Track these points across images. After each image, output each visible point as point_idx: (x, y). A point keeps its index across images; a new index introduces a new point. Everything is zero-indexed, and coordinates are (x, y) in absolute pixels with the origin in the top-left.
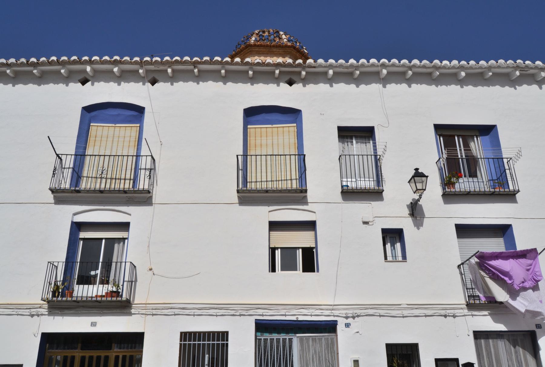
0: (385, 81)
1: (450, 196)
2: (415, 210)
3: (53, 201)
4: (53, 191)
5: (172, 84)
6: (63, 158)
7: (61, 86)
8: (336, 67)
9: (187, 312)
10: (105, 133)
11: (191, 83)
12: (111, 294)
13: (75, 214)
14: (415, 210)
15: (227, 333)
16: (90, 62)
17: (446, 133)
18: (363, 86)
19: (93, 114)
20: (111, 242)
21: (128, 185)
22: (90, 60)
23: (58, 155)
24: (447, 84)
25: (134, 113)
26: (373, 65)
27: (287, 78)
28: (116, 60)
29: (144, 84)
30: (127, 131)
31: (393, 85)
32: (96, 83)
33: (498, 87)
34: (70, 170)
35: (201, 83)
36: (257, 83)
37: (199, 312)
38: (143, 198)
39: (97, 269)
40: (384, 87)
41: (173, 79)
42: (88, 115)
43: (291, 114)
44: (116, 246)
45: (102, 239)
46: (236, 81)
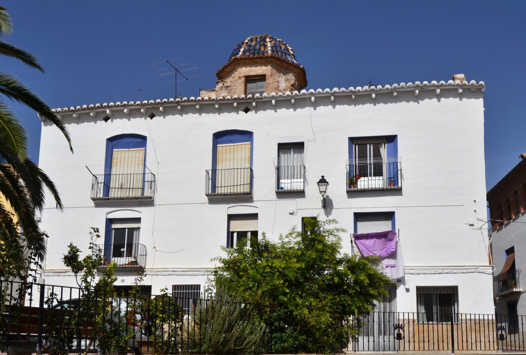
0: (315, 105)
1: (353, 192)
2: (327, 204)
3: (94, 206)
4: (93, 199)
5: (164, 118)
6: (97, 176)
7: (92, 123)
8: (277, 97)
9: (176, 273)
10: (123, 156)
11: (177, 116)
12: (132, 263)
13: (108, 214)
14: (327, 204)
15: (200, 285)
16: (108, 107)
17: (358, 143)
18: (299, 110)
19: (115, 142)
20: (131, 230)
21: (139, 194)
22: (108, 105)
23: (94, 175)
24: (364, 103)
25: (139, 141)
26: (304, 94)
27: (244, 107)
28: (125, 104)
29: (146, 119)
30: (135, 153)
31: (322, 107)
32: (114, 120)
33: (404, 103)
34: (102, 184)
35: (184, 115)
36: (223, 112)
37: (182, 273)
38: (148, 202)
39: (124, 247)
40: (315, 109)
41: (164, 114)
42: (111, 144)
43: (246, 135)
44: (135, 232)
45: (125, 228)
46: (208, 112)
